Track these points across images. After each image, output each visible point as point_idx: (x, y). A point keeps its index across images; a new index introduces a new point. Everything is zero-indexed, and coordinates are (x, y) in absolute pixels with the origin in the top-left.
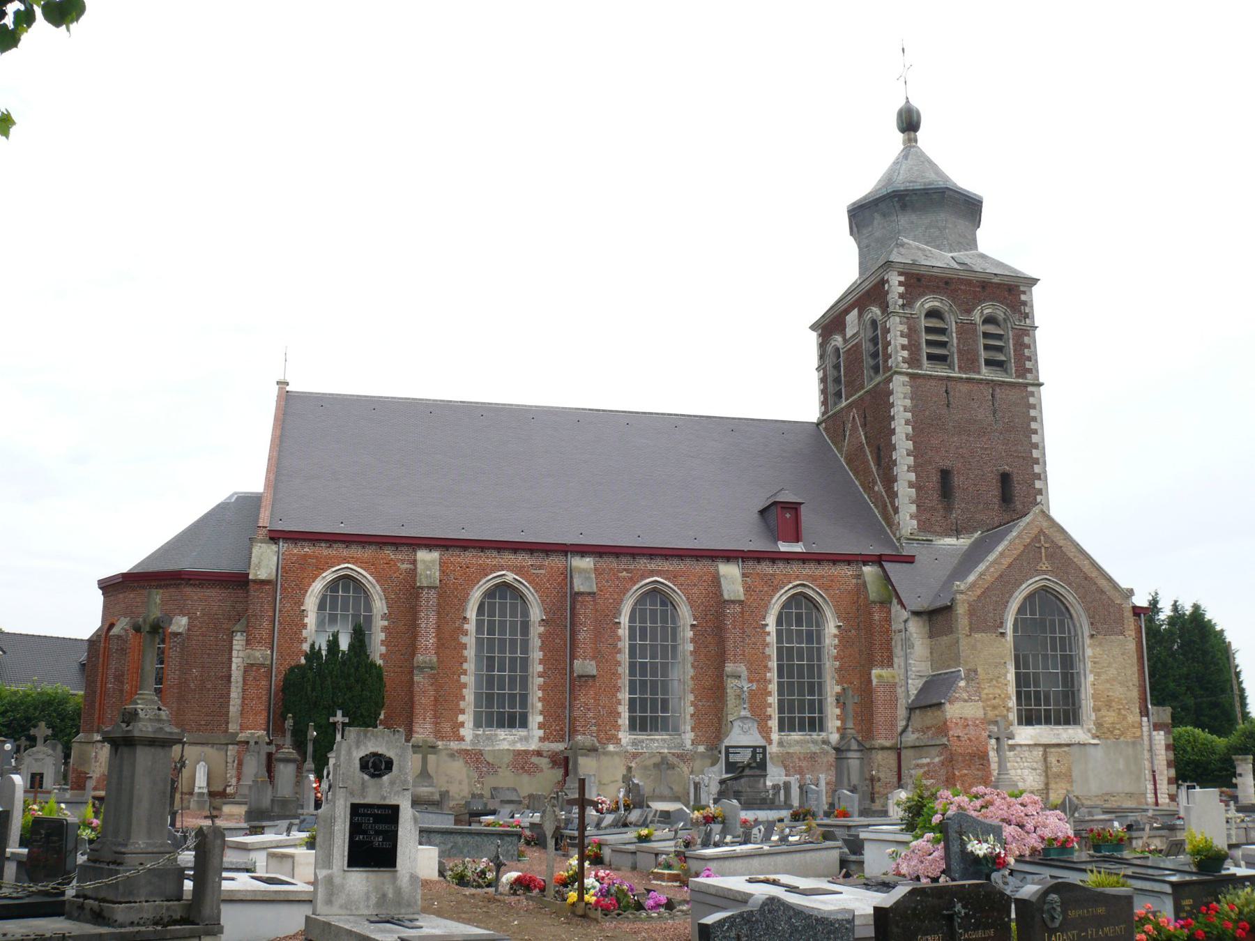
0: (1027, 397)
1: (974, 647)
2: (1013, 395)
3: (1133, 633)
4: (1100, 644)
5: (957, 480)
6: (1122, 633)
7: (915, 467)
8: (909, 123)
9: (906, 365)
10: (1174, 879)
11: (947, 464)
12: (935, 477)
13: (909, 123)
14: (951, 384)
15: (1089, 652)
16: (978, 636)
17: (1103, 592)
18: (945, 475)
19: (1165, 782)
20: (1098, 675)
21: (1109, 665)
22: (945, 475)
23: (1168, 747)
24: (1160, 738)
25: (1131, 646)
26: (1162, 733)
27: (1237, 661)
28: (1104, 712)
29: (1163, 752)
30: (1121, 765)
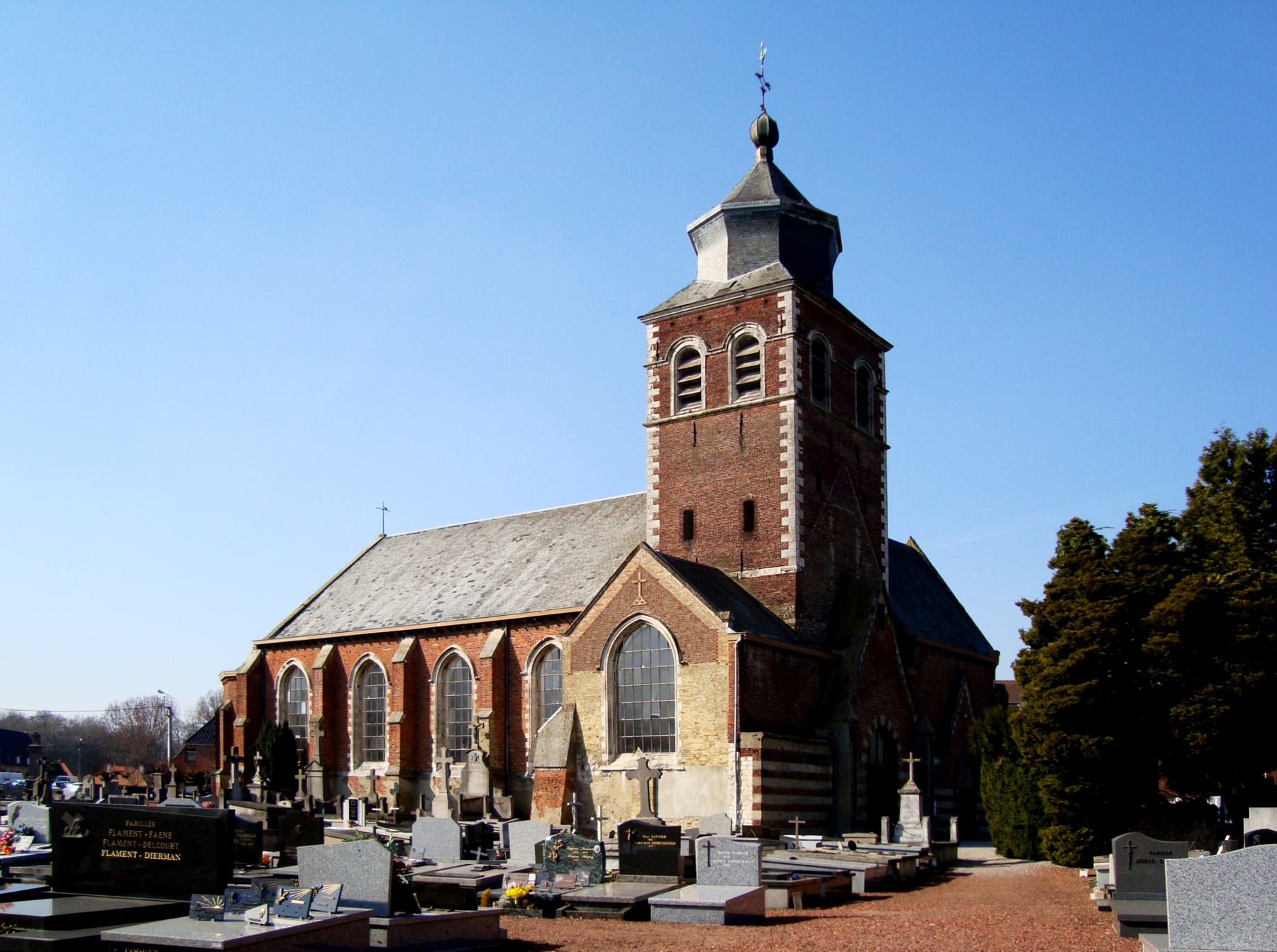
0: (778, 414)
1: (573, 685)
2: (763, 415)
3: (727, 659)
4: (691, 672)
5: (699, 518)
6: (715, 659)
7: (660, 514)
8: (768, 138)
9: (657, 416)
10: (125, 832)
11: (685, 505)
12: (678, 521)
13: (768, 138)
14: (698, 422)
15: (678, 682)
16: (577, 674)
17: (696, 619)
18: (689, 516)
19: (750, 806)
20: (686, 702)
21: (699, 692)
22: (689, 516)
23: (755, 773)
24: (749, 764)
25: (724, 671)
26: (750, 758)
27: (34, 714)
28: (690, 740)
29: (750, 778)
30: (705, 791)
